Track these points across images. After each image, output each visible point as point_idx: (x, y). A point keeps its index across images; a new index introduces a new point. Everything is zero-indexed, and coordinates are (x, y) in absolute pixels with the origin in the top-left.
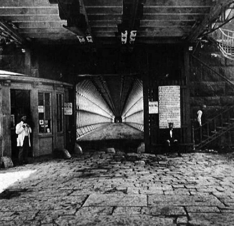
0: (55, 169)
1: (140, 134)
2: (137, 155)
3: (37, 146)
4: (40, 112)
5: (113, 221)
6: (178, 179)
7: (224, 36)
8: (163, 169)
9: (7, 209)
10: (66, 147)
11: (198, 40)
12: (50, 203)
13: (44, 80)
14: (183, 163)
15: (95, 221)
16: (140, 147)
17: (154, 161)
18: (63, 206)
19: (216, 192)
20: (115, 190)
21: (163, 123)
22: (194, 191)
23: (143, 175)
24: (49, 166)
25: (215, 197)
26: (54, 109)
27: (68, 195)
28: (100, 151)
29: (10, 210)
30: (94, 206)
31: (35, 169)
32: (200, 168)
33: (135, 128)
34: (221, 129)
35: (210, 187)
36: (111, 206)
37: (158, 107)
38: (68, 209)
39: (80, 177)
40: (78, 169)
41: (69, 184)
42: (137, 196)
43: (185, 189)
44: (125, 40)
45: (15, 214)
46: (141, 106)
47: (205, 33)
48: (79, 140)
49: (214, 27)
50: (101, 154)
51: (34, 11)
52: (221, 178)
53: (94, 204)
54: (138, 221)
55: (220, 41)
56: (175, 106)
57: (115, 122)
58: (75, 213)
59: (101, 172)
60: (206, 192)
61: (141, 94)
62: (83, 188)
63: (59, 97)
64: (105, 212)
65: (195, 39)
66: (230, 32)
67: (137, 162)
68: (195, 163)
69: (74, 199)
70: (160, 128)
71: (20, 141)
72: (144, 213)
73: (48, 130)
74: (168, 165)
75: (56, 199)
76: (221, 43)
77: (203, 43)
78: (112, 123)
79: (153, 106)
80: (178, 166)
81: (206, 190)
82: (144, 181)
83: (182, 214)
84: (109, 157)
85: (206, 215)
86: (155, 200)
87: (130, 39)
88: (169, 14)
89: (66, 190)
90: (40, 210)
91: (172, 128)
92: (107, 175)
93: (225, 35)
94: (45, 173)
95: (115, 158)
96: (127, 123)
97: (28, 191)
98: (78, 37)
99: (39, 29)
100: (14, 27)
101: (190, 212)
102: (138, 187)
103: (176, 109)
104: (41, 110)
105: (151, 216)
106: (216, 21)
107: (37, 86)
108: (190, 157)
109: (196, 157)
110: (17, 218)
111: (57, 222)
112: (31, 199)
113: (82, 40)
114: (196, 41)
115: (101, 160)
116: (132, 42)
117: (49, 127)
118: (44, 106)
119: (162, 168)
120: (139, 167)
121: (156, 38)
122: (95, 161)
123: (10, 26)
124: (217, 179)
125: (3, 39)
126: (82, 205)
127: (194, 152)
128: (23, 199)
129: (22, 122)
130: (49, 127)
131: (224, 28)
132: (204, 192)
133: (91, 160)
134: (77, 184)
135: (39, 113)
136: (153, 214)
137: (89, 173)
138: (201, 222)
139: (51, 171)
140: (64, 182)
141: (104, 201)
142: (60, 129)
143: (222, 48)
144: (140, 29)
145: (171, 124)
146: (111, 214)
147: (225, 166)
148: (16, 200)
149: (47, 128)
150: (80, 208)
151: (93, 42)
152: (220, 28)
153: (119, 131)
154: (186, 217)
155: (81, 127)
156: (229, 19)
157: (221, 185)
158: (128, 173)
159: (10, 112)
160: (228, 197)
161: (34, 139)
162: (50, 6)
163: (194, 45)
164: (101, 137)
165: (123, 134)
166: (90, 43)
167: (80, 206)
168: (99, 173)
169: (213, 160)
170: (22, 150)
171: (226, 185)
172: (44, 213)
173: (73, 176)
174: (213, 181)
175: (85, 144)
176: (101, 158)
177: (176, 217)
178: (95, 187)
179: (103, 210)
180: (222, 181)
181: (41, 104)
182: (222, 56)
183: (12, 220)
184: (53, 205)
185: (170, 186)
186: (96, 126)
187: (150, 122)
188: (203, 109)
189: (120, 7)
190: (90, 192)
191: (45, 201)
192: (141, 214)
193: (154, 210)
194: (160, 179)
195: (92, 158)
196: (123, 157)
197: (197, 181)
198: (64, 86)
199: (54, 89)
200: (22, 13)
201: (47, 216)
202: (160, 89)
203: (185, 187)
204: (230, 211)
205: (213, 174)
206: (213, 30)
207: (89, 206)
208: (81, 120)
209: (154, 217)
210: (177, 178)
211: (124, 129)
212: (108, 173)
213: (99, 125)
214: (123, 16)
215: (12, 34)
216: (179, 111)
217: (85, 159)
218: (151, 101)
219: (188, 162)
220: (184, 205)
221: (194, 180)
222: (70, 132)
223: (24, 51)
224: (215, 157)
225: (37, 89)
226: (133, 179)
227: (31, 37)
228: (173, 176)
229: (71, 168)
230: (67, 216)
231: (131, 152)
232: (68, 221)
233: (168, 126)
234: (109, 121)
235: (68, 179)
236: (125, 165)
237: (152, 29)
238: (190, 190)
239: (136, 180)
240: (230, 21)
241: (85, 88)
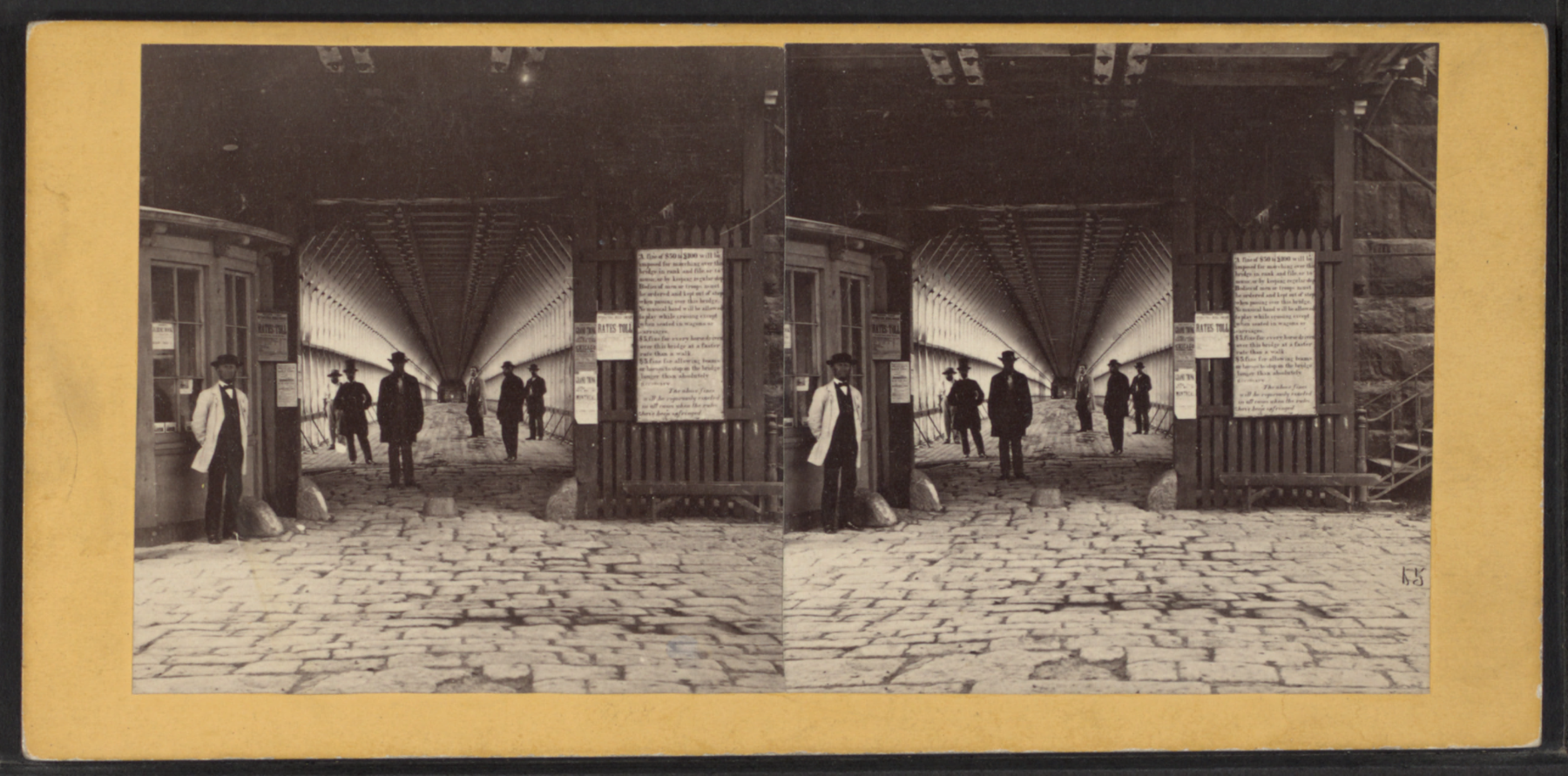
37: (1231, 331)
43: (1362, 661)
87: (1128, 65)
103: (1298, 340)
116: (1134, 77)
118: (174, 320)
199: (217, 255)
202: (645, 261)
203: (1362, 652)
238: (1387, 663)
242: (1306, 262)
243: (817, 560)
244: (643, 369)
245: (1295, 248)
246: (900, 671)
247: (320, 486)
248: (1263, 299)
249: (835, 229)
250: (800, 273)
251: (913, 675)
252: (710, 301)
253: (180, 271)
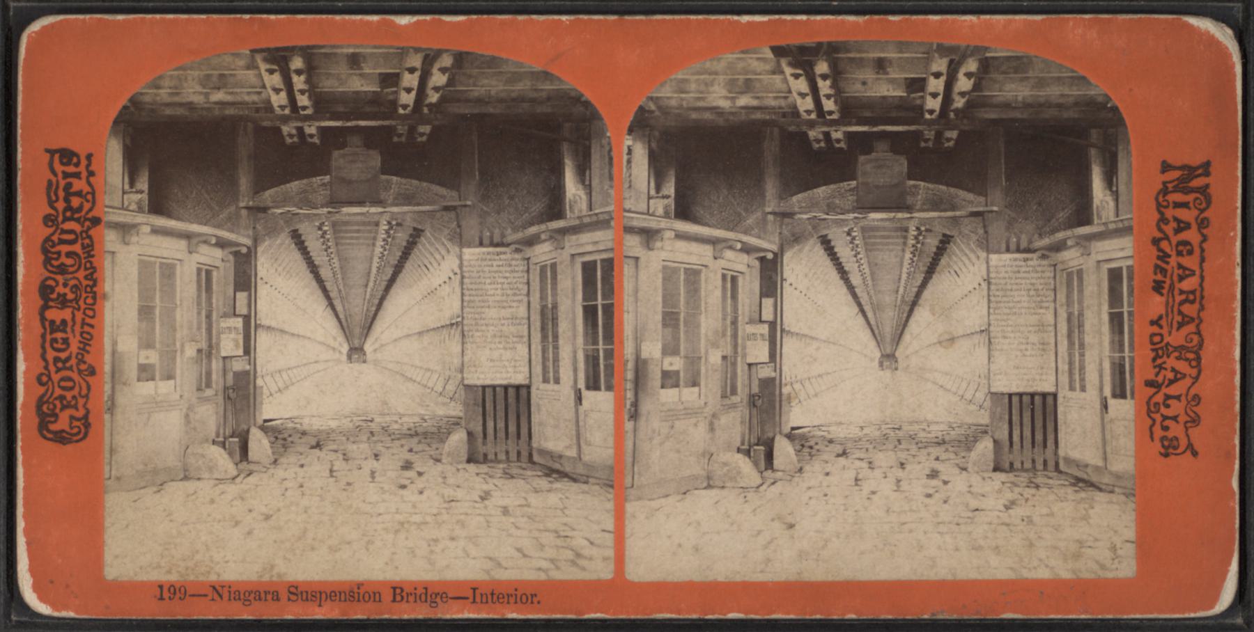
243: (135, 501)
248: (1012, 293)
250: (688, 269)
252: (1044, 295)
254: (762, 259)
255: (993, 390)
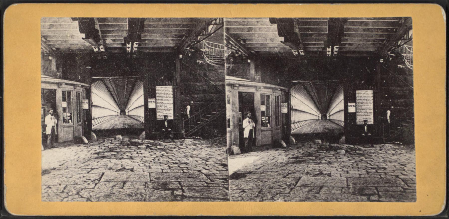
0: (273, 156)
1: (140, 124)
2: (339, 145)
3: (259, 137)
4: (262, 110)
5: (124, 193)
6: (371, 165)
7: (408, 51)
8: (359, 157)
9: (236, 188)
10: (283, 137)
11: (388, 54)
12: (270, 184)
13: (264, 85)
14: (176, 147)
15: (110, 193)
16: (341, 139)
17: (352, 150)
18: (85, 181)
19: (400, 175)
20: (321, 173)
21: (160, 115)
22: (186, 170)
23: (145, 157)
24: (269, 154)
25: (203, 174)
26: (74, 105)
27: (88, 173)
28: (110, 138)
29: (239, 189)
30: (305, 186)
31: (258, 156)
32: (190, 151)
33: (336, 124)
34: (205, 120)
35: (396, 171)
36: (318, 187)
37: (156, 102)
38: (89, 184)
39: (96, 158)
40: (94, 152)
41: (88, 164)
42: (339, 179)
44: (330, 53)
45: (242, 191)
46: (141, 101)
47: (192, 44)
48: (293, 133)
49: (400, 44)
50: (111, 140)
51: (258, 30)
52: (405, 164)
53: (108, 180)
54: (339, 199)
55: (203, 50)
56: (368, 107)
57: (322, 119)
58: (94, 187)
59: (310, 159)
60: (393, 176)
61: (341, 97)
62: (296, 172)
63: (277, 98)
64: (118, 186)
65: (184, 49)
66: (211, 44)
67: (339, 151)
68: (385, 152)
69: (290, 181)
70: (157, 119)
71: (246, 134)
72: (344, 192)
73: (268, 125)
74: (363, 154)
75: (78, 176)
76: (406, 57)
77: (391, 56)
78: (319, 119)
79: (151, 102)
80: (371, 155)
81: (393, 174)
82: (146, 162)
83: (177, 188)
84: (117, 143)
85: (197, 188)
86: (156, 177)
88: (364, 33)
89: (282, 173)
90: (262, 189)
91: (366, 124)
92: (315, 162)
93: (409, 50)
94: (266, 159)
95: (321, 148)
96: (332, 119)
97: (56, 169)
98: (293, 50)
99: (262, 45)
100: (242, 42)
101: (184, 186)
102: (340, 171)
104: (263, 108)
105: (154, 190)
106: (402, 39)
107: (61, 86)
108: (381, 147)
109: (185, 142)
110: (244, 195)
111: (80, 194)
112: (255, 180)
113: (296, 53)
114: (185, 50)
115: (310, 149)
116: (335, 55)
117: (269, 122)
119: (359, 156)
120: (141, 150)
121: (153, 48)
122: (306, 149)
123: (239, 42)
124: (402, 165)
125: (233, 52)
126: (295, 186)
127: (184, 138)
128: (248, 180)
129: (248, 119)
130: (269, 122)
131: (408, 45)
132: (392, 176)
133: (303, 149)
134: (94, 164)
135: (261, 111)
136: (155, 188)
137: (102, 155)
138: (193, 194)
139: (73, 153)
140: (84, 163)
141: (116, 178)
142: (277, 124)
143: (206, 56)
144: (342, 46)
145: (165, 116)
146: (122, 188)
147: (209, 150)
148: (244, 180)
149: (267, 123)
150: (293, 188)
151: (305, 54)
152: (405, 45)
153: (325, 126)
154: (377, 196)
155: (295, 123)
156: (211, 33)
157: (206, 165)
158: (332, 160)
159: (238, 110)
160: (410, 180)
161: (257, 132)
162: (271, 26)
163: (384, 58)
164: (310, 131)
165: (328, 129)
166: (303, 55)
167: (294, 186)
168: (110, 155)
169: (398, 150)
170: (50, 137)
171: (409, 170)
172: (266, 191)
173: (288, 162)
174: (398, 166)
175: (297, 136)
176: (111, 143)
177: (173, 190)
178: (108, 167)
179: (116, 185)
180: (406, 167)
181: (263, 103)
182: (205, 61)
183: (46, 193)
184: (272, 185)
185: (365, 171)
186: (307, 122)
187: (349, 119)
188: (191, 104)
189: (326, 27)
190: (302, 175)
191: (71, 177)
192: (342, 193)
193: (156, 185)
194: (159, 160)
195: (303, 148)
196: (328, 147)
197: (386, 167)
198: (82, 86)
199: (74, 89)
200: (248, 31)
201: (268, 194)
203: (179, 167)
204: (215, 185)
205: (200, 156)
206: (400, 46)
207: (105, 182)
208: (294, 117)
209: (156, 190)
210: (171, 159)
211: (128, 120)
212: (118, 155)
213: (309, 122)
214: (328, 35)
215: (240, 47)
216: (372, 111)
217: (298, 148)
218: (150, 98)
219: (180, 147)
220: (376, 185)
221: (384, 166)
222: (86, 123)
223: (249, 61)
224: (400, 147)
225: (62, 89)
226: (138, 160)
227: (255, 50)
228: (169, 157)
229: (287, 156)
230: (283, 194)
231: (334, 143)
232: (89, 193)
233: (163, 118)
234: (317, 118)
235: (87, 160)
236: (131, 149)
237: (350, 44)
238: (183, 168)
239: (140, 161)
240: (212, 35)
241: (298, 91)
242: (371, 93)
244: (158, 110)
245: (169, 85)
246: (91, 171)
247: (95, 133)
249: (75, 83)
251: (92, 172)
253: (266, 95)
254: (285, 92)
255: (240, 152)
